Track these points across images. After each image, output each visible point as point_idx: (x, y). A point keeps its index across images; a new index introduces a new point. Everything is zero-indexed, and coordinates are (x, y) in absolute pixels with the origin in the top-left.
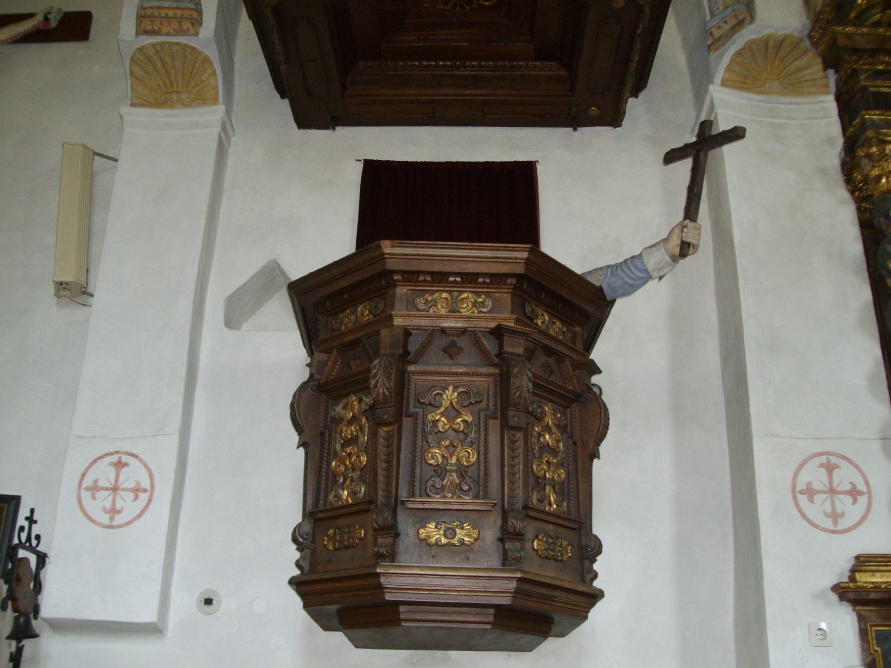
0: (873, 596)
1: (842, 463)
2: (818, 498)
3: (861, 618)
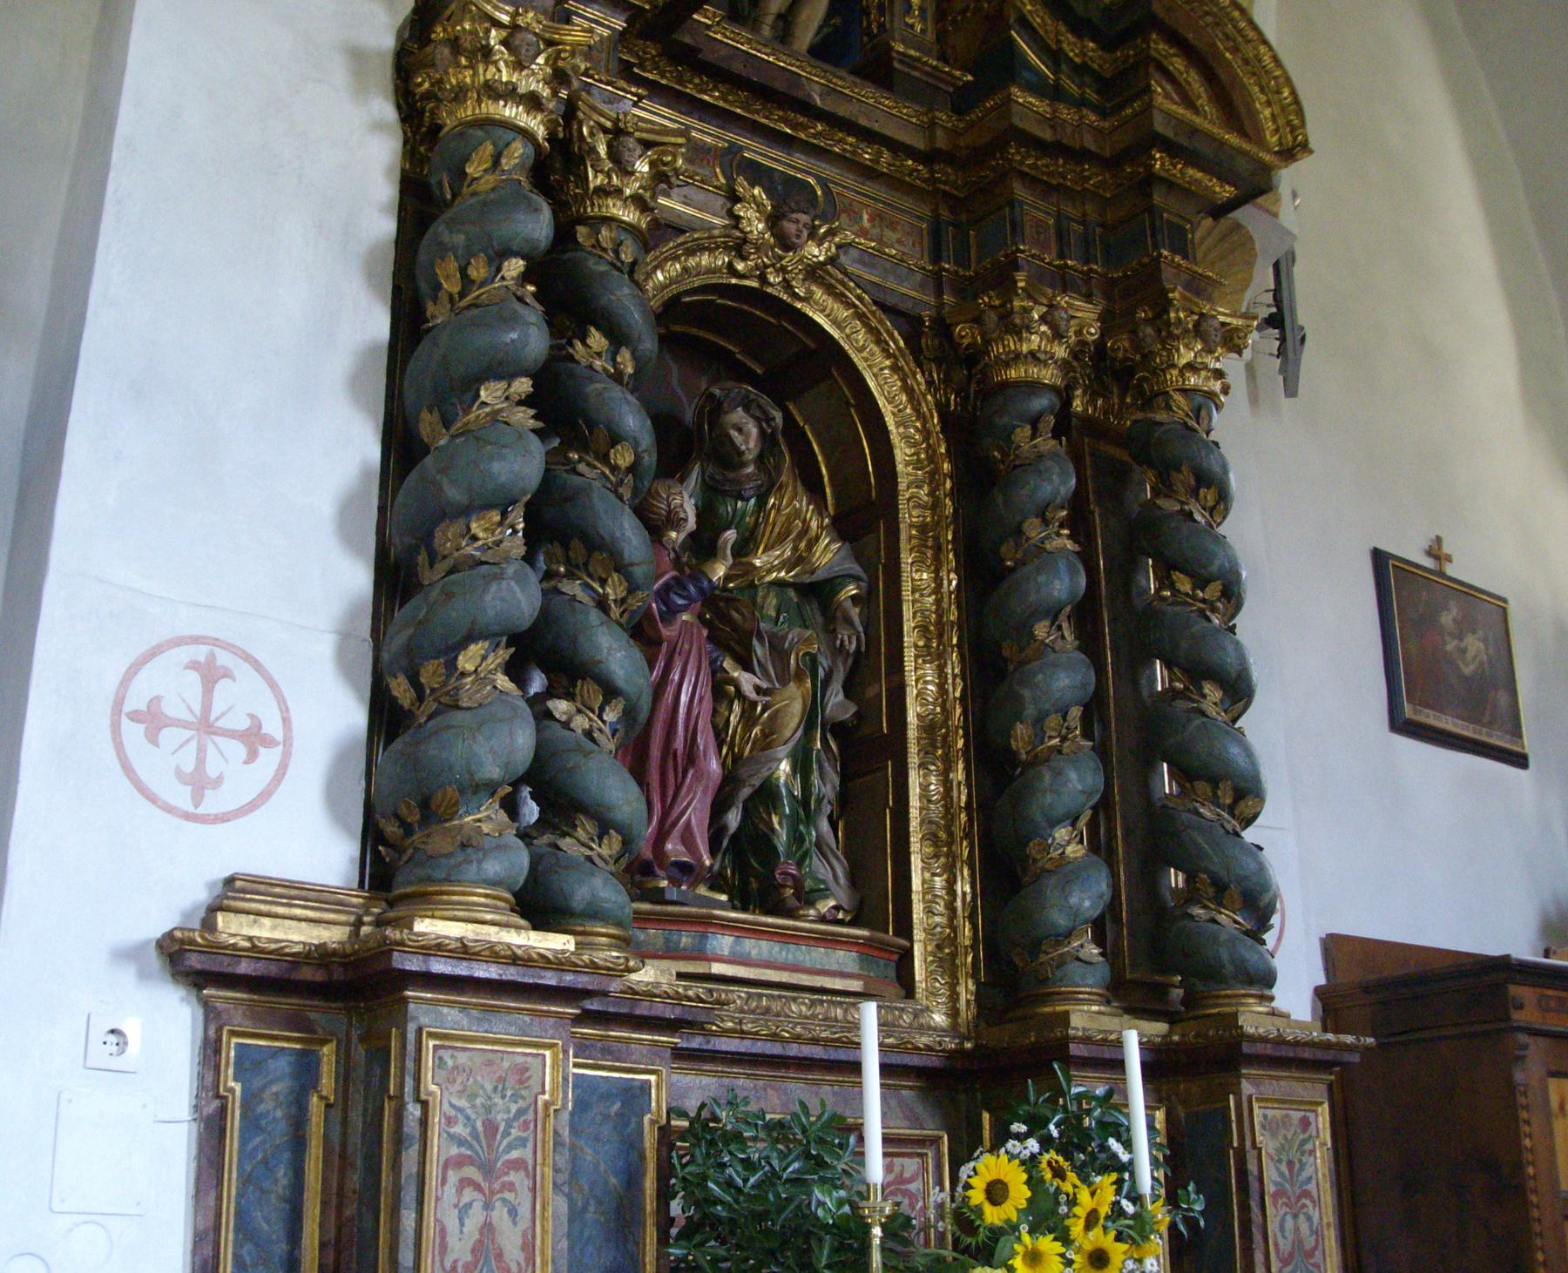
0: (244, 968)
1: (242, 669)
2: (169, 736)
3: (210, 1012)
